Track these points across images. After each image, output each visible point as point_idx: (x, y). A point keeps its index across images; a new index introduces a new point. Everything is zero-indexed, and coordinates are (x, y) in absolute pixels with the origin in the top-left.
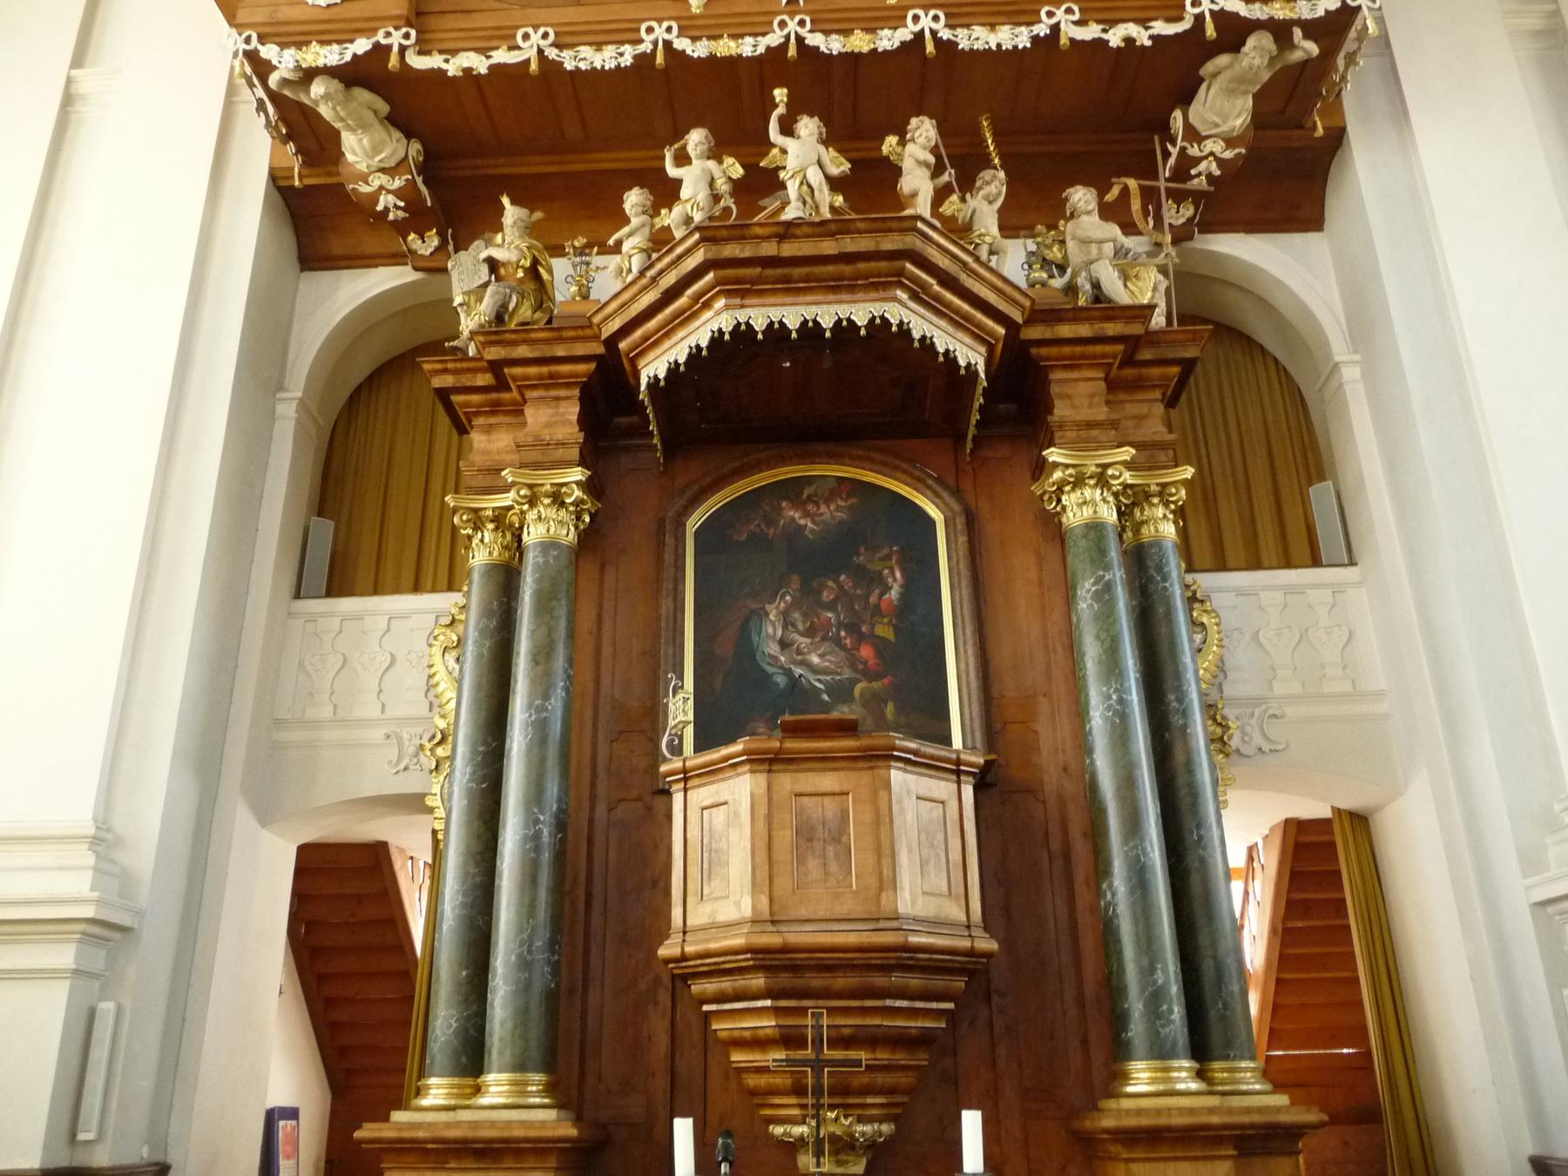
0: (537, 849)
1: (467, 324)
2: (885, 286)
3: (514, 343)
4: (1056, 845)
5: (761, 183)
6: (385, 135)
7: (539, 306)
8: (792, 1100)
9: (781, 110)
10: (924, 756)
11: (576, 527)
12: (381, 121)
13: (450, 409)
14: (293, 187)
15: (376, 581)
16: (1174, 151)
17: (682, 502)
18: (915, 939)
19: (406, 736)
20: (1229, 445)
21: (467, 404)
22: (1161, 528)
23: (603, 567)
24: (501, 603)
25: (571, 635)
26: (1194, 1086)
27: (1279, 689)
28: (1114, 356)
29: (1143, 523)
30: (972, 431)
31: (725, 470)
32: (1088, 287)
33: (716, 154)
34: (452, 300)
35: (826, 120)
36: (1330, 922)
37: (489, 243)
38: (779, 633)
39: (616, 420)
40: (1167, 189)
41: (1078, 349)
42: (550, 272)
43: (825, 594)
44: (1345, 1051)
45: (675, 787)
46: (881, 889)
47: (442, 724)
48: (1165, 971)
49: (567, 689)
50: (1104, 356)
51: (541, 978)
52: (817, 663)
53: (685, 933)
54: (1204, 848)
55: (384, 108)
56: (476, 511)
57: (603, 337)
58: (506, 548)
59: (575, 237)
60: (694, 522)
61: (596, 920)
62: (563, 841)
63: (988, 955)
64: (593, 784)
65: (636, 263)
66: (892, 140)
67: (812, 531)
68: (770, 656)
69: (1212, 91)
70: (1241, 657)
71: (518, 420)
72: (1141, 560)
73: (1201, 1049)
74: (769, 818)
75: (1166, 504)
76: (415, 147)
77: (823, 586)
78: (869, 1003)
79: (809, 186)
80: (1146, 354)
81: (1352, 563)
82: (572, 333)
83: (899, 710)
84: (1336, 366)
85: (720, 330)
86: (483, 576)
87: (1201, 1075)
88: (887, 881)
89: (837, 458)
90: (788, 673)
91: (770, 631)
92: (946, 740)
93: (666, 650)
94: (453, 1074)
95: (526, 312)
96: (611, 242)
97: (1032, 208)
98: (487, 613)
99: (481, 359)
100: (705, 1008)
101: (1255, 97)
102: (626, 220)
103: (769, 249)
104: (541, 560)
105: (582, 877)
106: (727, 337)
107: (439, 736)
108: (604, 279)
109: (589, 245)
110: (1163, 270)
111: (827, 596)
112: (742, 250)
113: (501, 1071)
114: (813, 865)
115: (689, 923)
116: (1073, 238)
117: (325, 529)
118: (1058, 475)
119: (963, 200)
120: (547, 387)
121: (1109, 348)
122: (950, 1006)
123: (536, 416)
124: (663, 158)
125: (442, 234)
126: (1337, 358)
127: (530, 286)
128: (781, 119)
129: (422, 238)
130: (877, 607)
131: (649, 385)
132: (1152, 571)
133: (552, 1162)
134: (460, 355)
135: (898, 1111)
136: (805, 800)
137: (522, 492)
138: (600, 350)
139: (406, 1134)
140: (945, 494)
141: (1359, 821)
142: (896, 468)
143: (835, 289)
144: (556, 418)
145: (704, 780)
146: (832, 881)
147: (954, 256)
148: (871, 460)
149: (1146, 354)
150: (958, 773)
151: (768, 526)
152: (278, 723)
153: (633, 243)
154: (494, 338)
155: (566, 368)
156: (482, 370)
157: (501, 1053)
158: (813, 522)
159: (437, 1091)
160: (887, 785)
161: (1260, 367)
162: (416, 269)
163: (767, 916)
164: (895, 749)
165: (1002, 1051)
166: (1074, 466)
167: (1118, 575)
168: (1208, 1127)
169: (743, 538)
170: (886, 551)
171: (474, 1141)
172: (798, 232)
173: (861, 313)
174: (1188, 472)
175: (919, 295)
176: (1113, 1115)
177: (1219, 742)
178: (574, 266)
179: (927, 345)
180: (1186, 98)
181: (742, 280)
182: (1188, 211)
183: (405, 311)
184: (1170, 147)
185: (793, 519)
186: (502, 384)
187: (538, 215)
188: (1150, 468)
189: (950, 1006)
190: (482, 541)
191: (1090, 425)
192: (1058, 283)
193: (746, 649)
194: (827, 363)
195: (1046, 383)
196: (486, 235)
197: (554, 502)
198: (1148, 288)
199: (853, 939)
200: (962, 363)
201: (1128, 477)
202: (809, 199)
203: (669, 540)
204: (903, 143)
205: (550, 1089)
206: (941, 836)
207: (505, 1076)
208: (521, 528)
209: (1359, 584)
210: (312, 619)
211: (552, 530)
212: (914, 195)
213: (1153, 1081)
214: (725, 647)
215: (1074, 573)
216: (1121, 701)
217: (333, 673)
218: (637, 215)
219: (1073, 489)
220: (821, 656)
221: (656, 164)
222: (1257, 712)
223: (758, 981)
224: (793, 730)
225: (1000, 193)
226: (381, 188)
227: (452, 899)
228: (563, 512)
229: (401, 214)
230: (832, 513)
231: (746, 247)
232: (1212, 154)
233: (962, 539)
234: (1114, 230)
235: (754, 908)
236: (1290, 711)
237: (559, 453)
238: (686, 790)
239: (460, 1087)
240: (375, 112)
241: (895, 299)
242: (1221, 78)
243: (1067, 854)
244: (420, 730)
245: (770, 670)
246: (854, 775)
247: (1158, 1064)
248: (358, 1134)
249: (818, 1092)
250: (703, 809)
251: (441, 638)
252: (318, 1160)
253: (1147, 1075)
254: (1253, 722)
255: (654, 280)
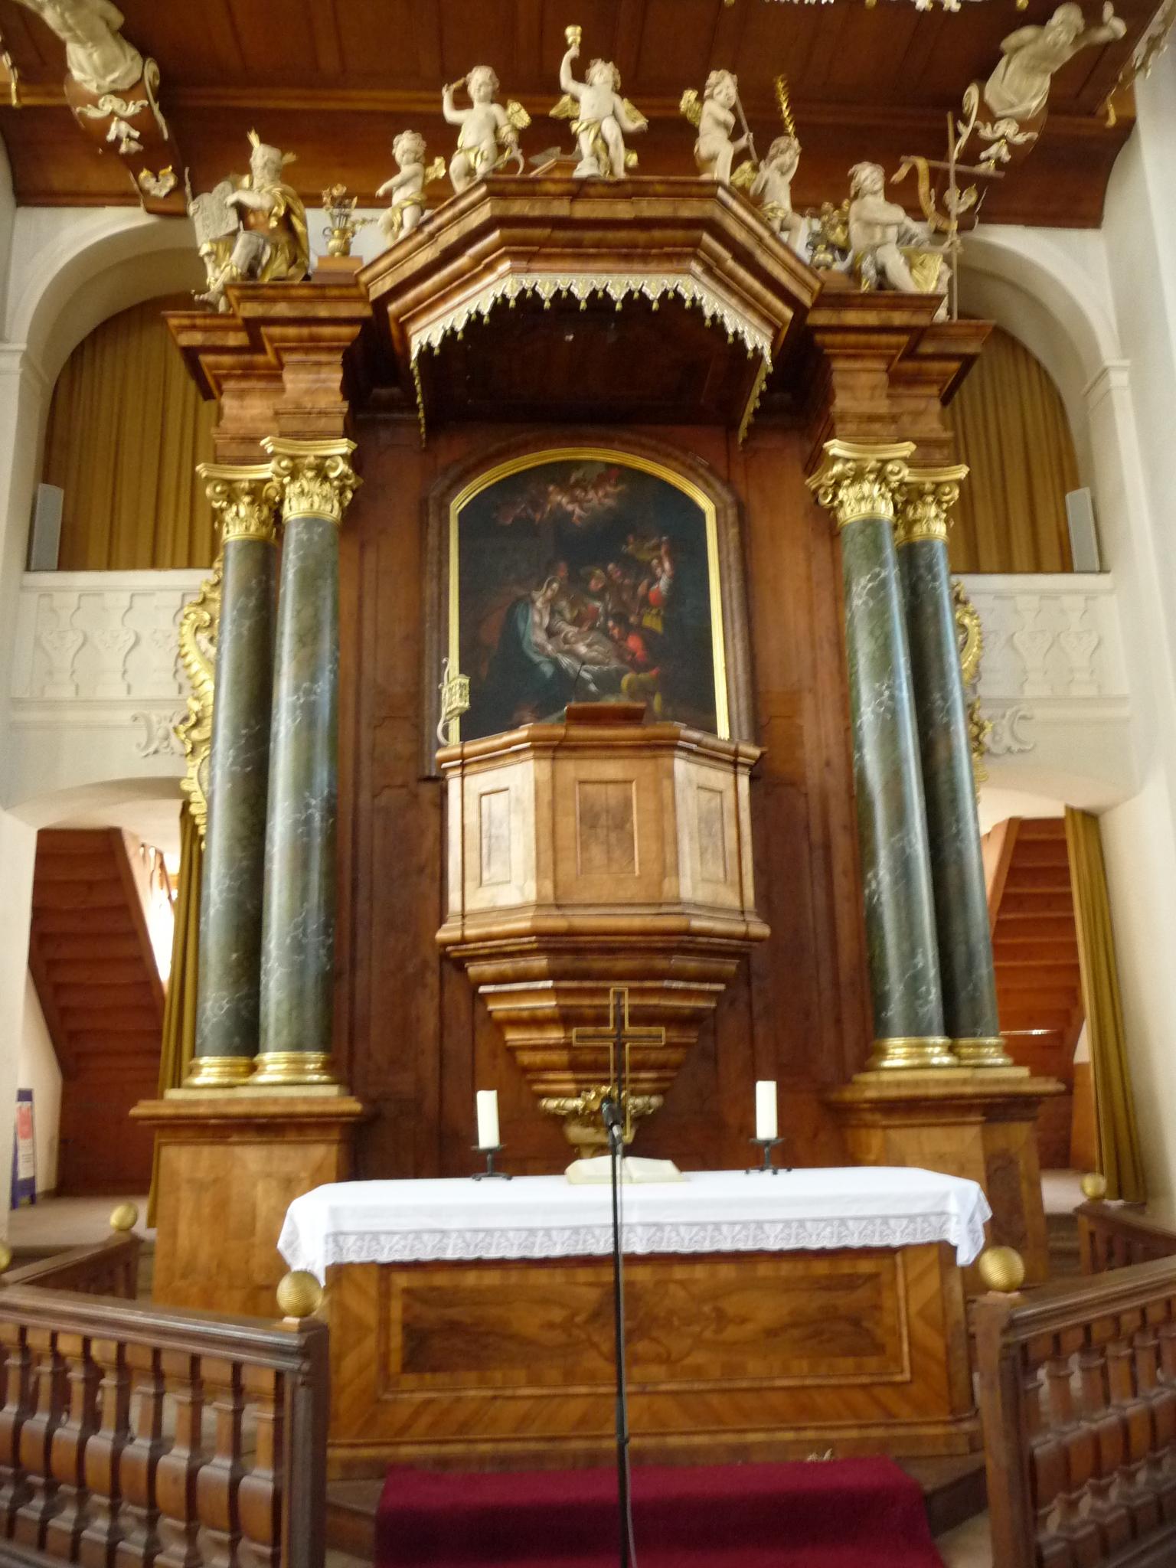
0: (308, 833)
1: (216, 278)
2: (680, 257)
3: (273, 300)
4: (816, 835)
5: (551, 133)
6: (117, 50)
7: (293, 262)
8: (568, 1076)
9: (573, 52)
10: (706, 747)
11: (341, 503)
12: (114, 33)
13: (196, 371)
14: (9, 107)
15: (110, 555)
16: (966, 132)
17: (447, 482)
18: (697, 924)
19: (154, 719)
20: (988, 445)
21: (217, 366)
22: (933, 528)
23: (362, 547)
24: (260, 582)
25: (336, 617)
26: (946, 1060)
27: (1030, 692)
28: (898, 347)
29: (915, 521)
30: (747, 419)
31: (491, 450)
32: (872, 272)
33: (500, 97)
34: (197, 250)
35: (622, 68)
36: (1041, 915)
37: (236, 187)
38: (546, 621)
39: (376, 391)
40: (958, 174)
41: (862, 338)
42: (304, 222)
43: (593, 583)
44: (1035, 1032)
45: (450, 774)
46: (663, 875)
47: (196, 706)
48: (925, 955)
49: (334, 672)
50: (889, 347)
51: (316, 960)
52: (584, 652)
53: (463, 916)
54: (962, 841)
55: (117, 19)
56: (230, 482)
57: (373, 297)
58: (263, 523)
59: (333, 185)
60: (459, 503)
61: (363, 907)
62: (334, 826)
63: (759, 939)
64: (357, 770)
65: (409, 217)
66: (690, 95)
67: (580, 518)
68: (537, 645)
69: (1012, 67)
70: (996, 660)
71: (274, 385)
72: (912, 556)
73: (952, 1028)
74: (553, 805)
75: (939, 503)
76: (151, 68)
77: (591, 575)
78: (649, 984)
79: (605, 141)
80: (927, 348)
81: (1103, 570)
82: (335, 292)
83: (666, 702)
84: (1105, 371)
85: (503, 296)
86: (239, 551)
87: (951, 1050)
88: (670, 868)
89: (607, 442)
90: (555, 663)
91: (537, 618)
92: (712, 729)
93: (431, 637)
94: (224, 1054)
95: (280, 267)
96: (381, 192)
97: (821, 185)
98: (245, 591)
99: (234, 316)
100: (482, 989)
101: (1053, 78)
102: (395, 169)
103: (561, 209)
104: (305, 537)
105: (348, 863)
106: (512, 303)
107: (193, 719)
108: (370, 236)
109: (349, 196)
110: (947, 260)
111: (595, 585)
112: (532, 207)
113: (278, 1049)
114: (597, 853)
115: (468, 907)
116: (858, 219)
117: (53, 497)
118: (838, 468)
119: (756, 168)
120: (307, 351)
121: (893, 339)
122: (720, 987)
123: (295, 382)
124: (440, 102)
125: (178, 173)
126: (1107, 363)
127: (283, 238)
128: (574, 63)
129: (156, 175)
130: (645, 597)
131: (421, 353)
132: (922, 571)
133: (335, 1135)
134: (209, 311)
135: (666, 1085)
136: (588, 788)
137: (284, 463)
138: (367, 312)
139: (184, 1111)
140: (718, 486)
141: (1090, 820)
142: (668, 456)
143: (627, 258)
144: (316, 384)
145: (483, 766)
146: (615, 868)
147: (750, 230)
148: (643, 446)
149: (927, 348)
150: (735, 764)
151: (535, 511)
152: (17, 703)
153: (404, 193)
154: (250, 292)
155: (327, 331)
156: (236, 329)
157: (278, 1034)
158: (582, 508)
159: (210, 1070)
160: (671, 775)
161: (1023, 373)
162: (150, 211)
163: (551, 900)
164: (678, 738)
165: (760, 1030)
166: (854, 460)
167: (891, 572)
168: (961, 1097)
169: (509, 521)
170: (654, 542)
171: (257, 1116)
172: (592, 191)
173: (653, 285)
174: (962, 472)
175: (713, 270)
176: (871, 1086)
177: (976, 743)
178: (332, 216)
179: (718, 325)
180: (983, 74)
181: (529, 240)
182: (970, 198)
183: (127, 263)
184: (961, 126)
185: (559, 504)
186: (256, 346)
187: (290, 158)
188: (925, 466)
189: (720, 987)
190: (237, 514)
191: (872, 418)
192: (840, 266)
193: (512, 638)
194: (612, 338)
195: (827, 372)
196: (232, 177)
197: (317, 476)
198: (930, 277)
199: (637, 923)
200: (750, 346)
201: (906, 474)
202: (603, 156)
203: (433, 520)
204: (700, 99)
205: (328, 1067)
206: (718, 826)
207: (282, 1055)
208: (282, 502)
209: (1111, 592)
210: (47, 593)
211: (316, 506)
212: (713, 158)
213: (909, 1056)
214: (491, 633)
215: (849, 570)
216: (892, 697)
217: (71, 653)
218: (408, 163)
219: (852, 484)
220: (589, 646)
221: (433, 108)
222: (1008, 713)
223: (540, 963)
224: (578, 717)
225: (792, 165)
226: (113, 114)
227: (218, 883)
228: (327, 487)
229: (135, 146)
230: (601, 499)
231: (532, 210)
232: (1003, 137)
233: (733, 532)
234: (897, 213)
235: (539, 892)
236: (1039, 713)
237: (322, 423)
238: (463, 776)
239: (231, 1065)
240: (108, 23)
241: (688, 272)
242: (1023, 52)
243: (827, 847)
244: (169, 713)
245: (537, 658)
246: (636, 763)
247: (914, 1040)
248: (134, 1112)
249: (620, 1067)
250: (482, 795)
251: (192, 617)
252: (52, 1139)
253: (904, 1050)
254: (1004, 722)
255: (432, 236)
